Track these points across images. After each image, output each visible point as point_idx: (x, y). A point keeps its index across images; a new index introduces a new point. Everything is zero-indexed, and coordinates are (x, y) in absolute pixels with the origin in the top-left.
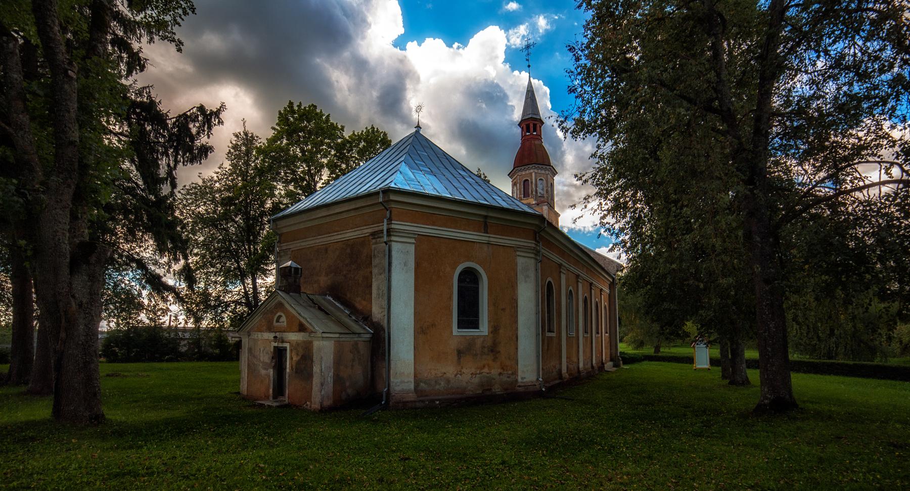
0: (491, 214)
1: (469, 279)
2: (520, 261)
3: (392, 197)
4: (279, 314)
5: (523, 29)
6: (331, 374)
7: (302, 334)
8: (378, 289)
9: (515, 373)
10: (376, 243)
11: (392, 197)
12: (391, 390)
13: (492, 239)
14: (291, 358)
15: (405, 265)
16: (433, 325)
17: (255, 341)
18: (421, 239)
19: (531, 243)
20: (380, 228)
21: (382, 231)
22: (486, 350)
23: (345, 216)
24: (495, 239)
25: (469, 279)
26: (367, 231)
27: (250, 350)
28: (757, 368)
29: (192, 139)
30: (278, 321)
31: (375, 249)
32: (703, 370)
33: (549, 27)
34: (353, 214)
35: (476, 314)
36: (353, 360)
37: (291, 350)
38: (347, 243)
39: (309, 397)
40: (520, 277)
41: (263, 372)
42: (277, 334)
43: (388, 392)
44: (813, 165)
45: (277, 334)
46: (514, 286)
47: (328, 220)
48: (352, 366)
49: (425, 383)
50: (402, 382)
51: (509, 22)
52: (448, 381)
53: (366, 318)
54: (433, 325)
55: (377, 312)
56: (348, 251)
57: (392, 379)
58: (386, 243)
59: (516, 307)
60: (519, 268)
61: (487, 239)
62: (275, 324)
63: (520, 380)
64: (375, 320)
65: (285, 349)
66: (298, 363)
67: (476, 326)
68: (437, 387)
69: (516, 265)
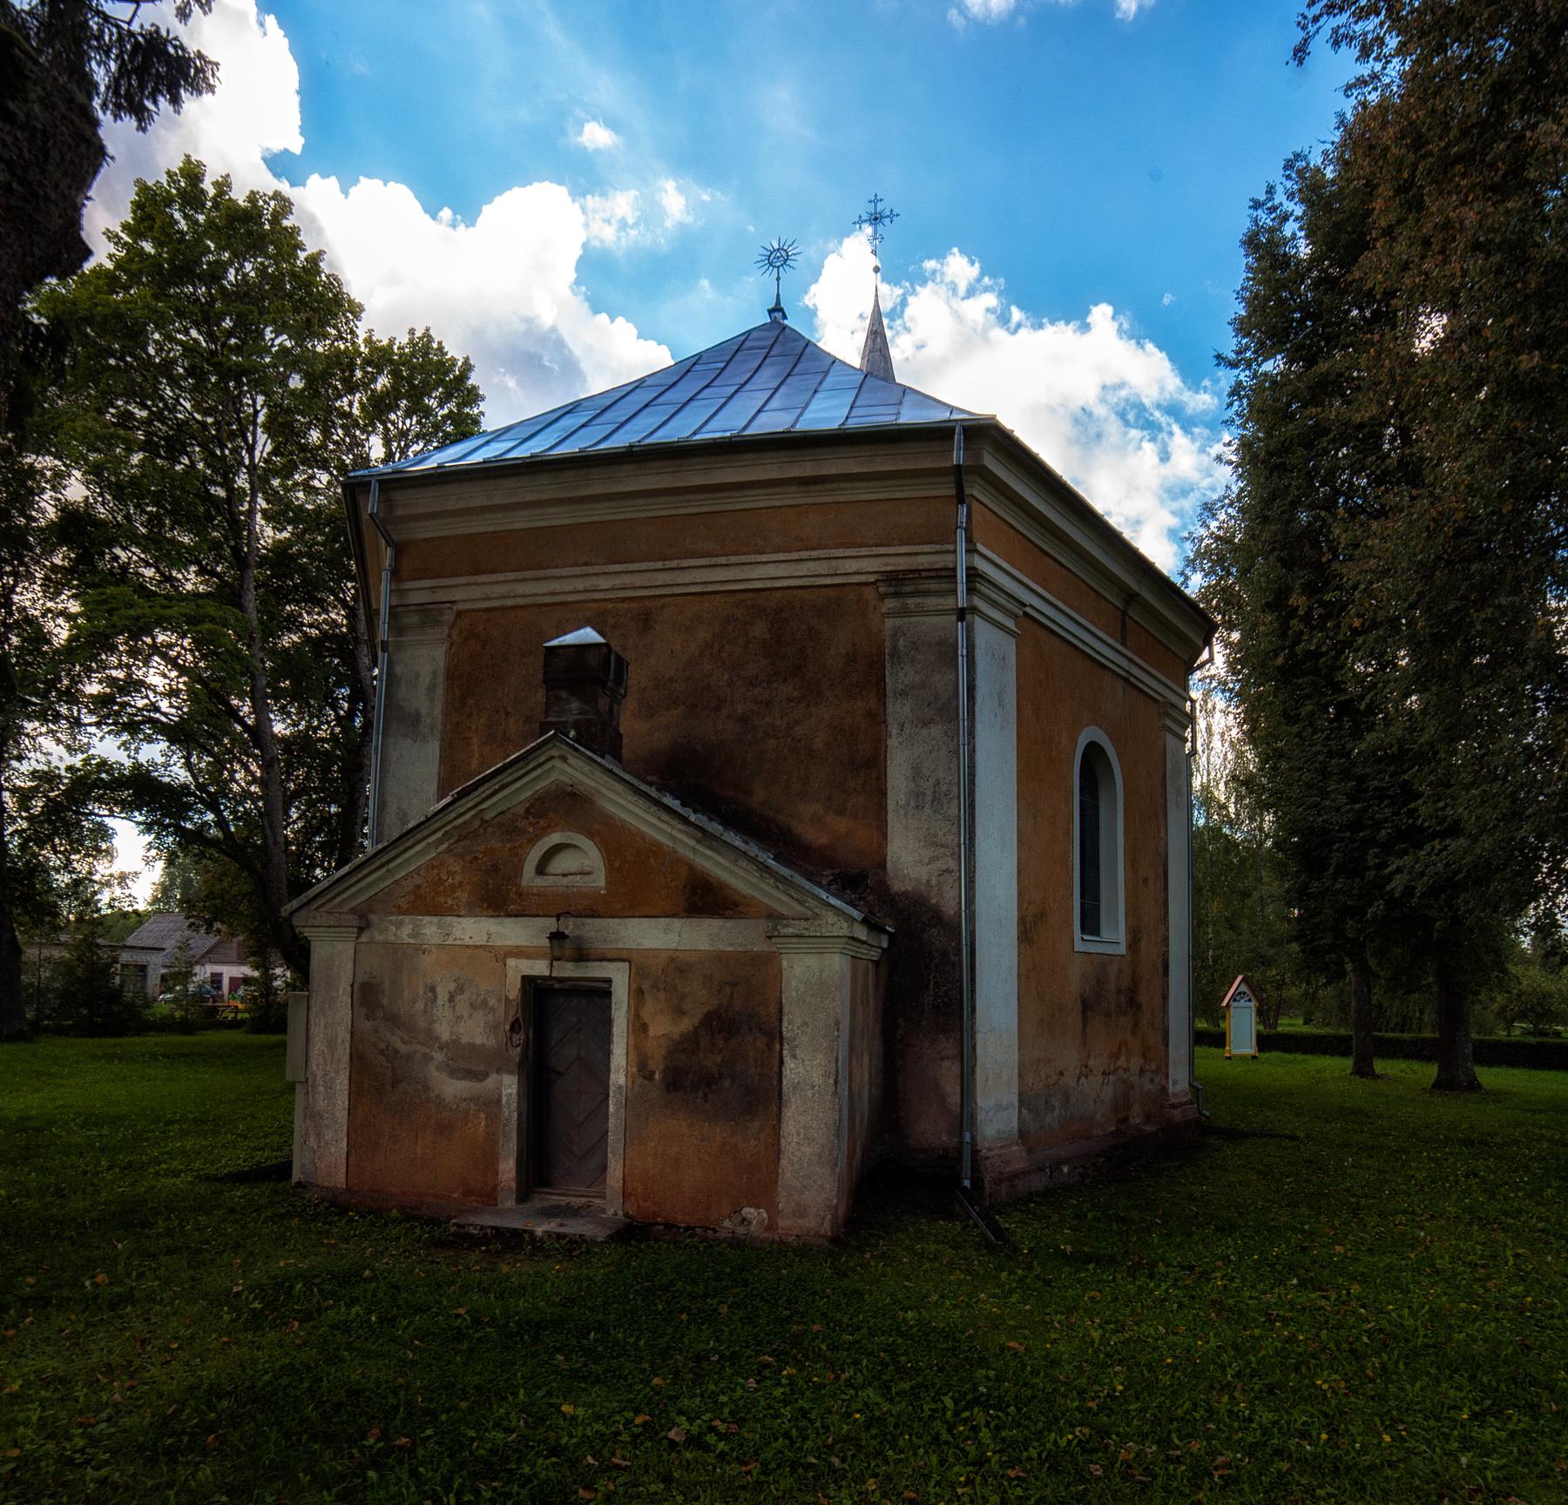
0: (1147, 595)
3: (990, 462)
4: (556, 838)
5: (623, 204)
7: (714, 924)
8: (916, 774)
10: (904, 612)
11: (990, 462)
14: (639, 1027)
17: (404, 957)
20: (940, 561)
21: (951, 574)
23: (760, 500)
26: (860, 565)
27: (367, 995)
28: (1344, 1053)
30: (541, 870)
31: (896, 632)
32: (1242, 1058)
33: (690, 219)
34: (791, 497)
37: (637, 995)
38: (753, 601)
39: (760, 1181)
41: (452, 1088)
42: (569, 926)
45: (569, 926)
47: (662, 508)
51: (584, 176)
53: (859, 880)
55: (908, 857)
56: (760, 629)
58: (961, 614)
62: (528, 877)
64: (897, 886)
65: (600, 993)
66: (686, 1046)
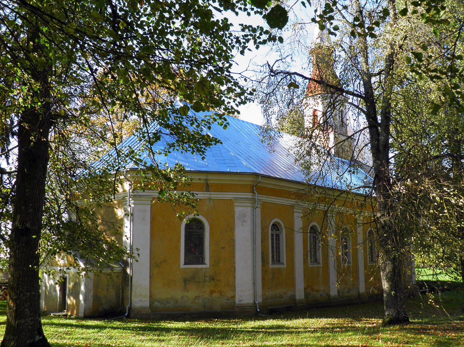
1: (195, 232)
2: (238, 210)
6: (91, 294)
9: (234, 297)
12: (133, 306)
13: (212, 196)
15: (143, 220)
16: (165, 261)
18: (264, 205)
19: (249, 195)
22: (208, 279)
24: (215, 195)
25: (195, 232)
29: (391, 186)
35: (202, 252)
36: (108, 285)
37: (69, 279)
40: (238, 222)
43: (130, 309)
44: (96, 50)
46: (231, 228)
48: (107, 289)
49: (158, 302)
50: (141, 301)
52: (177, 301)
54: (165, 261)
57: (133, 298)
59: (234, 246)
60: (237, 215)
61: (208, 196)
63: (237, 302)
67: (203, 263)
68: (168, 305)
69: (234, 213)
